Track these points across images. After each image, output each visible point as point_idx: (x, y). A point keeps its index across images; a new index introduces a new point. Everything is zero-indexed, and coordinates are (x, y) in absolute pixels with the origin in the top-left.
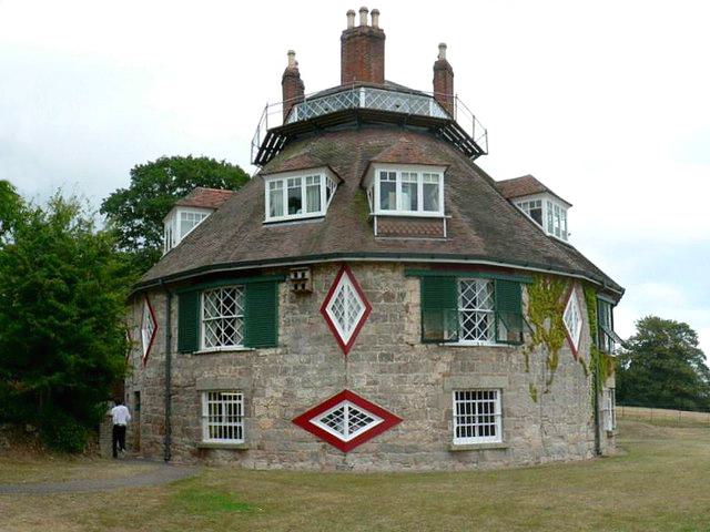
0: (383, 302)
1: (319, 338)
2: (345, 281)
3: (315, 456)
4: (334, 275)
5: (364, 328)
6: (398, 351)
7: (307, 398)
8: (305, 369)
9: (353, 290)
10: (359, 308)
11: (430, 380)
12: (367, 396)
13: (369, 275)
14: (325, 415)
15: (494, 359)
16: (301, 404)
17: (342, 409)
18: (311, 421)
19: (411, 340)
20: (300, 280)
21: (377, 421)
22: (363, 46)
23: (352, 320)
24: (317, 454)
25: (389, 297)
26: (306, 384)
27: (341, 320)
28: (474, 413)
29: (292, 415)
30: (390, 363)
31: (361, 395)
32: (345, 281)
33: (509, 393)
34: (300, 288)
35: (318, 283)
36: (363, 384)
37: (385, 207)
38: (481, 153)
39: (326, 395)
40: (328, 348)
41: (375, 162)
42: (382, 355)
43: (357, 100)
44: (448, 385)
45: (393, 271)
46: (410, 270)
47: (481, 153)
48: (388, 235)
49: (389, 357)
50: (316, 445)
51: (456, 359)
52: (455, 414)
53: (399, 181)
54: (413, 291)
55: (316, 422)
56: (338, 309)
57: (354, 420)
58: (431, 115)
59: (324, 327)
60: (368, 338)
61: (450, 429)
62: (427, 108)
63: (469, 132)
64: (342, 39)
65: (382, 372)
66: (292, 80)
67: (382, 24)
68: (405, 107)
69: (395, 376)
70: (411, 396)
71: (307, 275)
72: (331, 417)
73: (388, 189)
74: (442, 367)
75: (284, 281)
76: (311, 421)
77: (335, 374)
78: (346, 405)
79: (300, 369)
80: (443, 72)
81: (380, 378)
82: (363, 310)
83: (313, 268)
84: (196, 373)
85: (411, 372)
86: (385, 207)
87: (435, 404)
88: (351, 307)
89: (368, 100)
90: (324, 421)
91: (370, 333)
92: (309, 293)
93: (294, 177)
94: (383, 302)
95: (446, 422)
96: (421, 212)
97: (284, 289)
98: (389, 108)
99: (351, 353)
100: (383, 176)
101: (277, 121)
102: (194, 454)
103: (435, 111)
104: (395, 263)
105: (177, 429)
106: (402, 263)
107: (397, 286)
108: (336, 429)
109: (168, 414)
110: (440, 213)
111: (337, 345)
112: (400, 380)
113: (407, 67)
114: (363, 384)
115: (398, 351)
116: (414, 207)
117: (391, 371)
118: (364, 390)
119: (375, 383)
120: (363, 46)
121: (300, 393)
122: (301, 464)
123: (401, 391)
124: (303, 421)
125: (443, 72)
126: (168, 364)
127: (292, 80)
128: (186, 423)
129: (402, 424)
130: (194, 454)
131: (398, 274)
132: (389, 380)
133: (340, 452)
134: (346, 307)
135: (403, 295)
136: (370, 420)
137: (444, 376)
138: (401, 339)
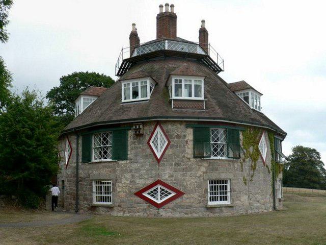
0: (176, 139)
1: (146, 156)
2: (158, 129)
3: (145, 210)
4: (153, 127)
5: (167, 151)
6: (183, 161)
7: (141, 183)
8: (140, 170)
9: (162, 134)
10: (165, 142)
11: (197, 175)
12: (169, 183)
13: (170, 127)
14: (149, 191)
15: (227, 165)
16: (138, 186)
17: (157, 188)
18: (143, 194)
19: (189, 157)
20: (138, 129)
21: (173, 194)
22: (167, 21)
23: (162, 147)
24: (145, 209)
25: (178, 137)
26: (141, 177)
27: (156, 148)
28: (218, 190)
29: (134, 191)
30: (179, 167)
31: (166, 182)
32: (158, 129)
33: (234, 181)
34: (138, 133)
35: (146, 130)
36: (167, 177)
37: (176, 95)
38: (221, 70)
39: (150, 182)
40: (150, 160)
41: (172, 74)
42: (175, 164)
43: (164, 46)
44: (206, 177)
45: (181, 125)
46: (188, 124)
47: (221, 70)
48: (178, 108)
49: (178, 165)
50: (145, 205)
51: (209, 165)
52: (209, 191)
53: (183, 84)
54: (190, 134)
55: (145, 194)
56: (155, 142)
57: (163, 194)
58: (198, 53)
59: (149, 150)
60: (169, 156)
61: (206, 197)
62: (196, 50)
63: (215, 61)
64: (157, 18)
65: (175, 171)
66: (134, 37)
67: (176, 11)
68: (186, 49)
69: (182, 173)
70: (189, 183)
71: (141, 126)
72: (152, 192)
73: (178, 87)
74: (203, 169)
75: (130, 129)
76: (143, 194)
77: (154, 172)
78: (159, 186)
79: (138, 170)
80: (203, 33)
81: (175, 174)
82: (167, 143)
83: (144, 123)
84: (90, 172)
85: (189, 171)
86: (176, 95)
87: (199, 186)
88: (161, 141)
89: (169, 46)
90: (149, 194)
91: (170, 153)
92: (142, 135)
93: (135, 81)
94: (176, 139)
95: (205, 194)
96: (193, 98)
97: (131, 133)
98: (179, 50)
99: (161, 162)
100: (176, 81)
101: (127, 55)
102: (89, 209)
103: (200, 51)
104: (181, 121)
105: (81, 198)
106: (185, 121)
107: (182, 132)
108: (154, 197)
109: (77, 190)
110: (202, 98)
111: (155, 159)
112: (184, 175)
113: (187, 31)
114: (167, 177)
115: (183, 161)
116: (190, 95)
117: (180, 171)
118: (167, 180)
119: (172, 176)
120: (167, 21)
121: (138, 181)
122: (138, 214)
123: (184, 180)
124: (139, 194)
125: (203, 33)
126: (77, 168)
127: (134, 37)
128: (85, 195)
129: (185, 195)
130: (89, 209)
131: (183, 127)
132: (179, 175)
133: (156, 208)
134: (159, 141)
135: (185, 136)
136: (170, 193)
137: (204, 173)
138: (184, 156)
